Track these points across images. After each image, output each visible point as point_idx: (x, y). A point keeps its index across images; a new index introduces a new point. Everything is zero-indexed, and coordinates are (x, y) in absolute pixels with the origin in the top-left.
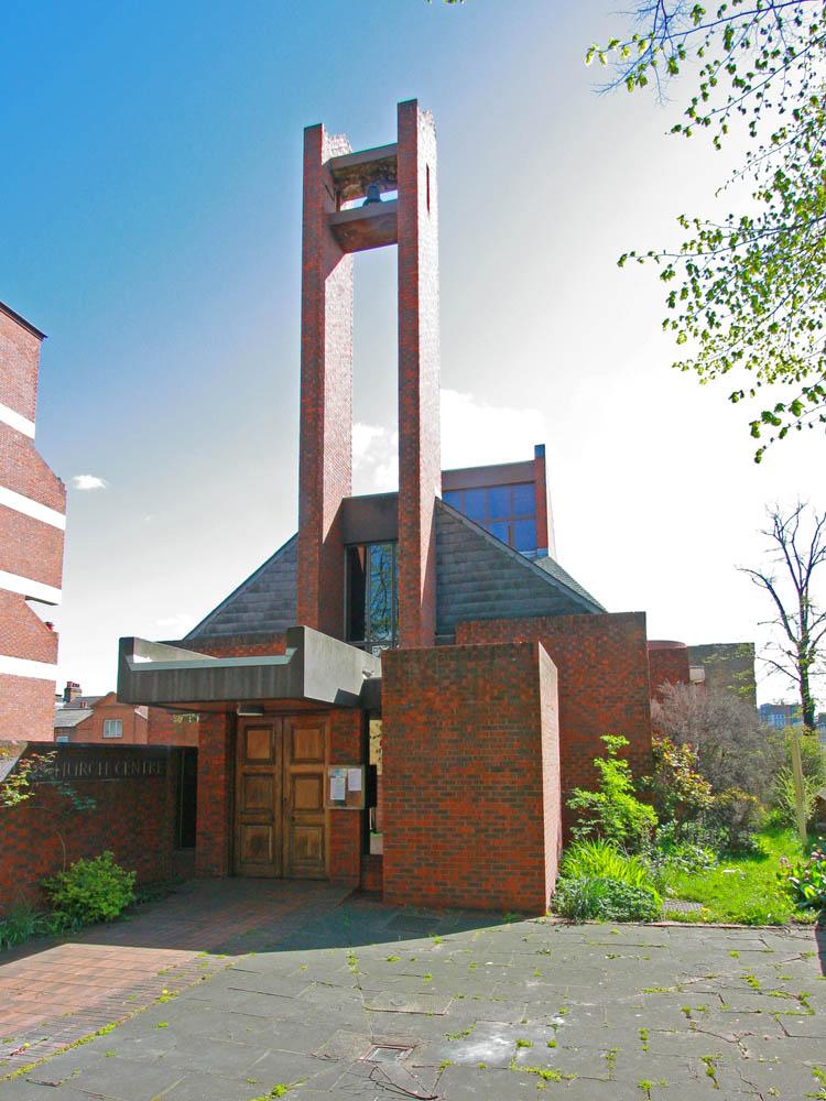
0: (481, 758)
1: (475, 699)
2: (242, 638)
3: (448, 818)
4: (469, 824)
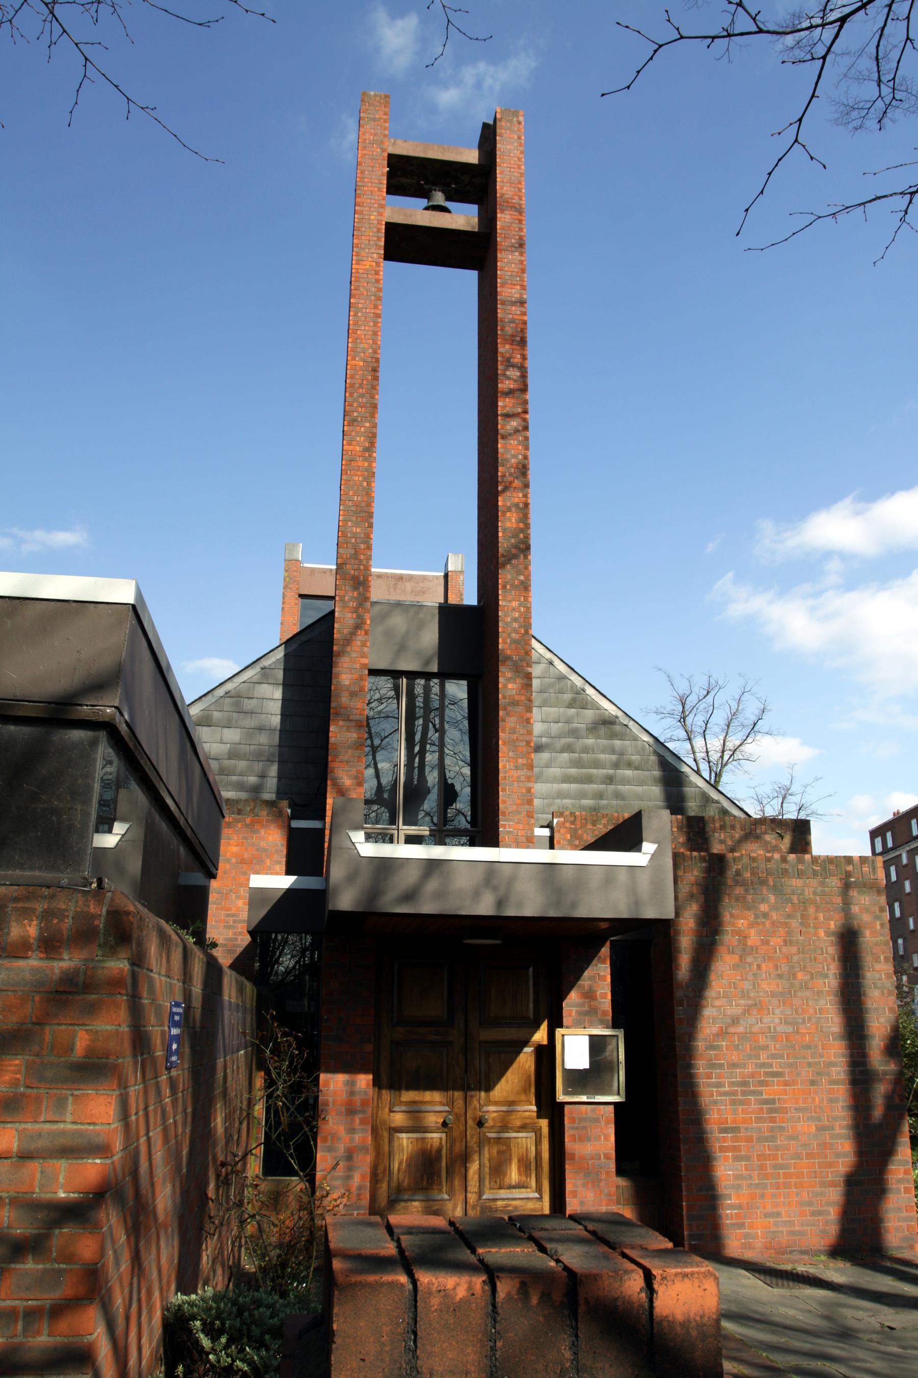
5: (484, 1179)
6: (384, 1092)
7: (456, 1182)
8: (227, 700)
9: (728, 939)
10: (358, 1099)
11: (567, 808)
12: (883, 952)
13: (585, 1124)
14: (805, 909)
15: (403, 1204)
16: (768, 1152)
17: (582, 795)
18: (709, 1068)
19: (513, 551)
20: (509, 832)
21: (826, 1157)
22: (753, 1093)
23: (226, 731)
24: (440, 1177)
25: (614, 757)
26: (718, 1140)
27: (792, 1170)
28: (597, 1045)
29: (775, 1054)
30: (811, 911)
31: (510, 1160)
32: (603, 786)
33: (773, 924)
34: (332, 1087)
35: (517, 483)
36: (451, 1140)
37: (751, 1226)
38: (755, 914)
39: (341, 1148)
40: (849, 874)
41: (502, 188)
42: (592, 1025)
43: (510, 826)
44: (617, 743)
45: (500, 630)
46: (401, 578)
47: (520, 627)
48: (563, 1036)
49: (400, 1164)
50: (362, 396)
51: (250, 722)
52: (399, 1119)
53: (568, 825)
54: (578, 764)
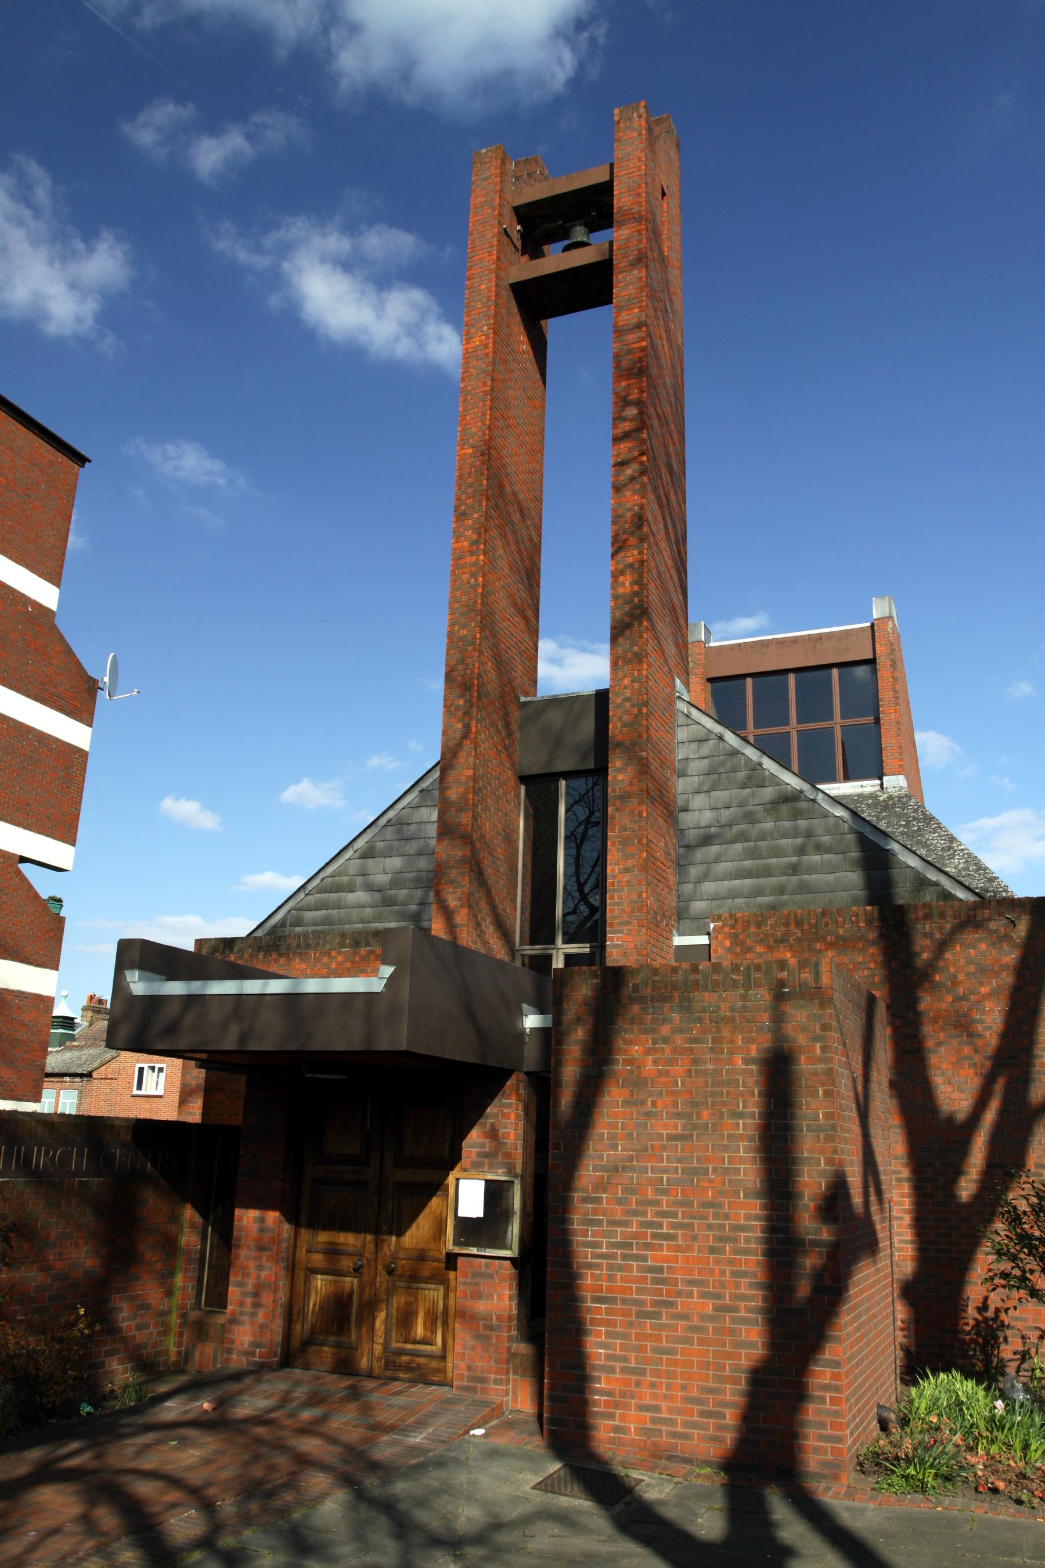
0: (727, 1171)
1: (716, 1061)
2: (343, 935)
3: (662, 1281)
4: (702, 1295)
5: (391, 1330)
6: (303, 1230)
7: (364, 1330)
8: (390, 829)
9: (620, 1066)
10: (267, 1236)
11: (740, 908)
12: (823, 1085)
13: (477, 1280)
14: (719, 1030)
15: (314, 1348)
16: (649, 1331)
17: (759, 892)
18: (584, 1224)
19: (627, 619)
20: (617, 946)
21: (724, 1346)
22: (636, 1258)
23: (388, 860)
24: (349, 1323)
25: (799, 841)
26: (594, 1311)
27: (679, 1357)
28: (494, 1194)
29: (667, 1212)
30: (726, 1033)
31: (417, 1313)
32: (784, 879)
33: (675, 1051)
34: (245, 1223)
35: (632, 540)
36: (362, 1287)
37: (623, 1418)
38: (653, 1039)
39: (251, 1282)
40: (781, 983)
41: (619, 200)
42: (492, 1168)
43: (618, 939)
44: (802, 823)
45: (611, 714)
46: (820, 637)
47: (632, 706)
48: (458, 1180)
49: (314, 1306)
50: (470, 486)
51: (413, 847)
52: (318, 1259)
53: (727, 930)
54: (753, 854)
